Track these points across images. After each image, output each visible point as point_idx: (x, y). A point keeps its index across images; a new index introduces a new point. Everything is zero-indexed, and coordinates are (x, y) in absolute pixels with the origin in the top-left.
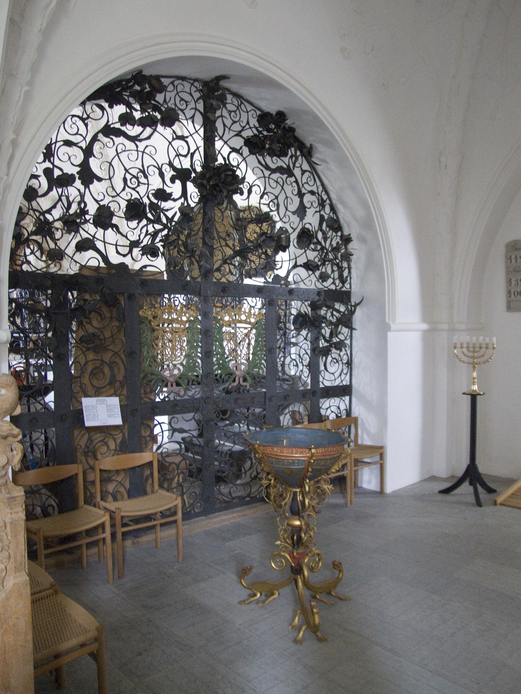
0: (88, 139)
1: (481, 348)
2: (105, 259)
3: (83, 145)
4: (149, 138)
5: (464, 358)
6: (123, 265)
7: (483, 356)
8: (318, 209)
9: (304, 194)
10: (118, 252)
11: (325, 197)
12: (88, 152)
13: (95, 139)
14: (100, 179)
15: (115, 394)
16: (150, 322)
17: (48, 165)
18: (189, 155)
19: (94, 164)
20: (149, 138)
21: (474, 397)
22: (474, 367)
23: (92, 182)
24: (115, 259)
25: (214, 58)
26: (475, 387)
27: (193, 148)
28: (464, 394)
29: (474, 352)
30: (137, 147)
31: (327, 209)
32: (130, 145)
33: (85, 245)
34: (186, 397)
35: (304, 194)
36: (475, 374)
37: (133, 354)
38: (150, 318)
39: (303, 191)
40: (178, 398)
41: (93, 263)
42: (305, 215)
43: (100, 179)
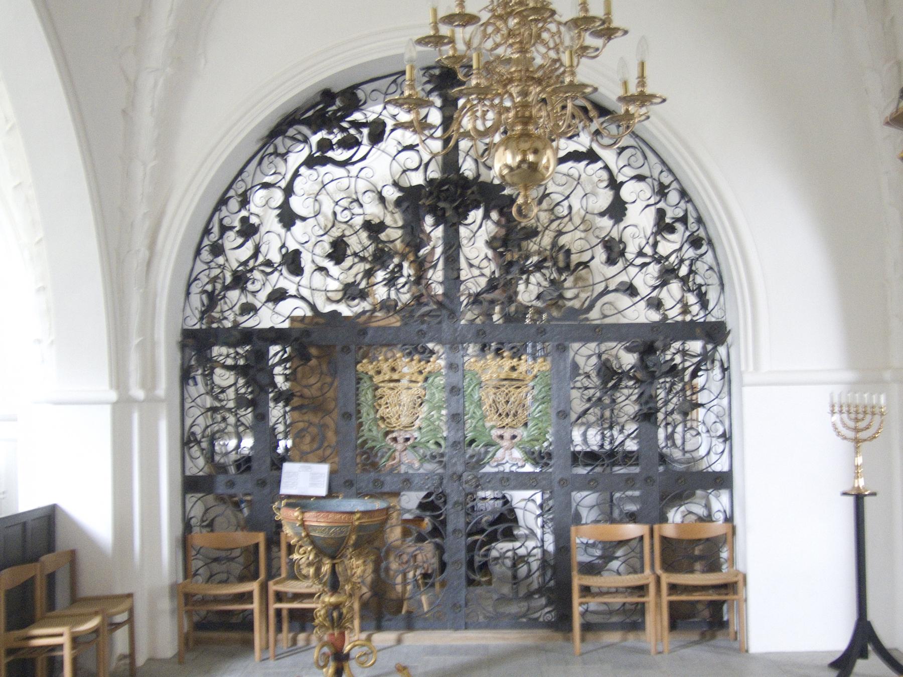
0: (288, 177)
1: (865, 413)
2: (313, 307)
3: (283, 184)
4: (364, 158)
5: (844, 431)
6: (335, 314)
7: (867, 428)
8: (652, 201)
9: (622, 183)
10: (328, 299)
11: (666, 179)
12: (289, 191)
13: (296, 174)
14: (304, 219)
15: (322, 460)
16: (371, 378)
17: (244, 213)
18: (422, 167)
19: (297, 205)
20: (364, 158)
21: (859, 499)
22: (857, 448)
23: (294, 224)
24: (326, 308)
25: (372, 61)
26: (861, 483)
27: (426, 158)
28: (845, 494)
29: (857, 420)
30: (349, 171)
31: (673, 196)
32: (339, 172)
33: (278, 296)
34: (421, 471)
35: (622, 183)
36: (859, 460)
37: (352, 415)
38: (371, 373)
39: (620, 179)
40: (411, 472)
41: (299, 313)
42: (625, 215)
43: (304, 219)
